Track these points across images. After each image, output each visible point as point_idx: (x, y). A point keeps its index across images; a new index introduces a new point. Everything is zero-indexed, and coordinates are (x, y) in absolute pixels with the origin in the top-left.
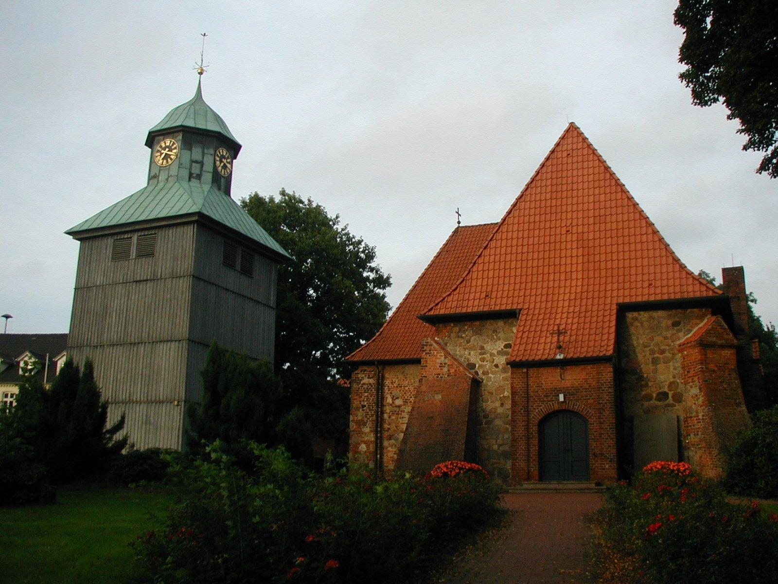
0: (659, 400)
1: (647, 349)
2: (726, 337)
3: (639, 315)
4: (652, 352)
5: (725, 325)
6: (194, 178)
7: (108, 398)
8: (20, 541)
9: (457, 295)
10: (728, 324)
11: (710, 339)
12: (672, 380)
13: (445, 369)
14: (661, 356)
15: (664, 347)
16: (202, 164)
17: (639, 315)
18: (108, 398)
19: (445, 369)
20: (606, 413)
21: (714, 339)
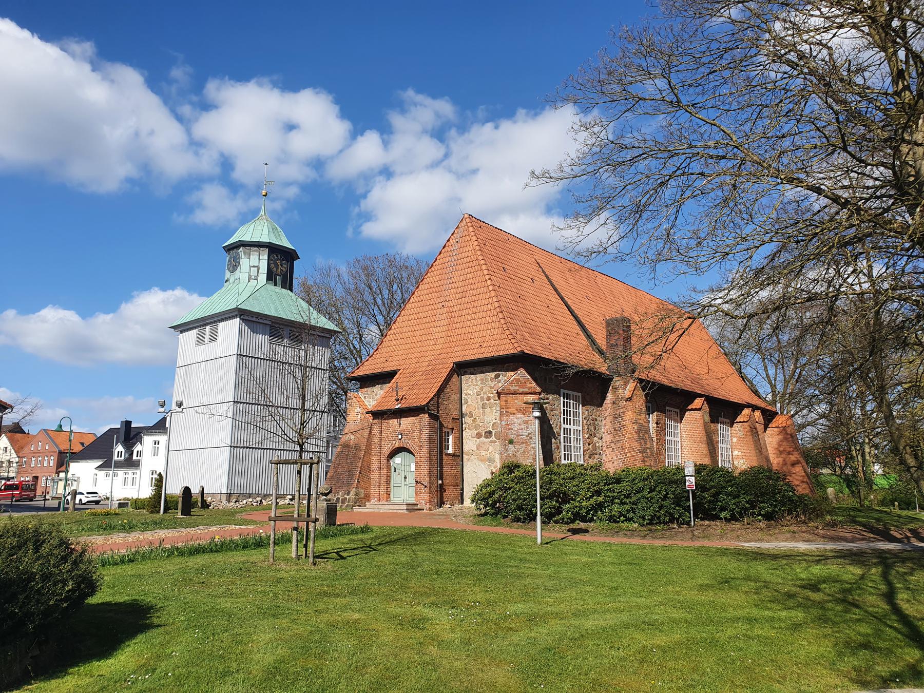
0: (486, 437)
1: (479, 397)
2: (529, 385)
3: (475, 370)
4: (482, 399)
5: (527, 375)
6: (252, 279)
7: (795, 585)
8: (30, 626)
9: (657, 149)
10: (530, 375)
11: (512, 388)
12: (494, 421)
13: (359, 416)
14: (488, 402)
15: (489, 395)
16: (258, 267)
17: (475, 370)
18: (795, 585)
19: (359, 416)
20: (424, 449)
21: (517, 388)
